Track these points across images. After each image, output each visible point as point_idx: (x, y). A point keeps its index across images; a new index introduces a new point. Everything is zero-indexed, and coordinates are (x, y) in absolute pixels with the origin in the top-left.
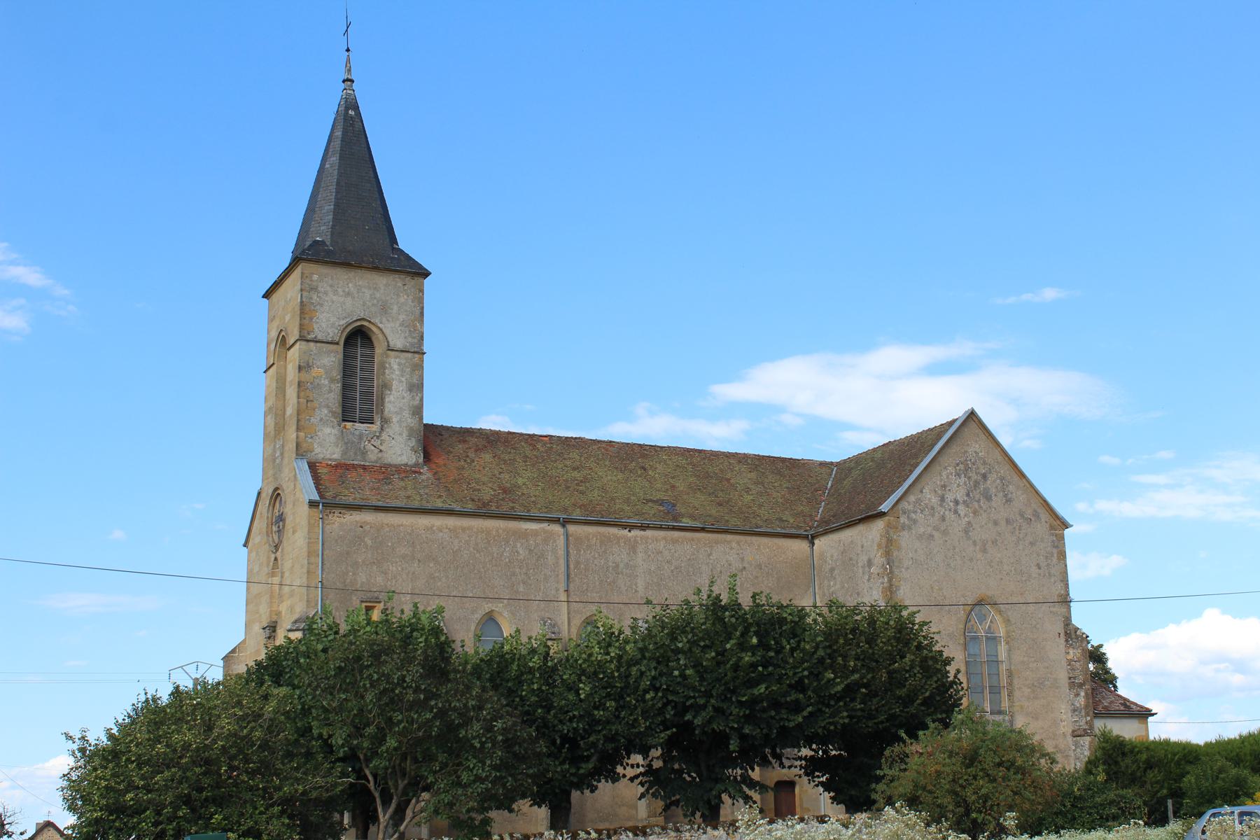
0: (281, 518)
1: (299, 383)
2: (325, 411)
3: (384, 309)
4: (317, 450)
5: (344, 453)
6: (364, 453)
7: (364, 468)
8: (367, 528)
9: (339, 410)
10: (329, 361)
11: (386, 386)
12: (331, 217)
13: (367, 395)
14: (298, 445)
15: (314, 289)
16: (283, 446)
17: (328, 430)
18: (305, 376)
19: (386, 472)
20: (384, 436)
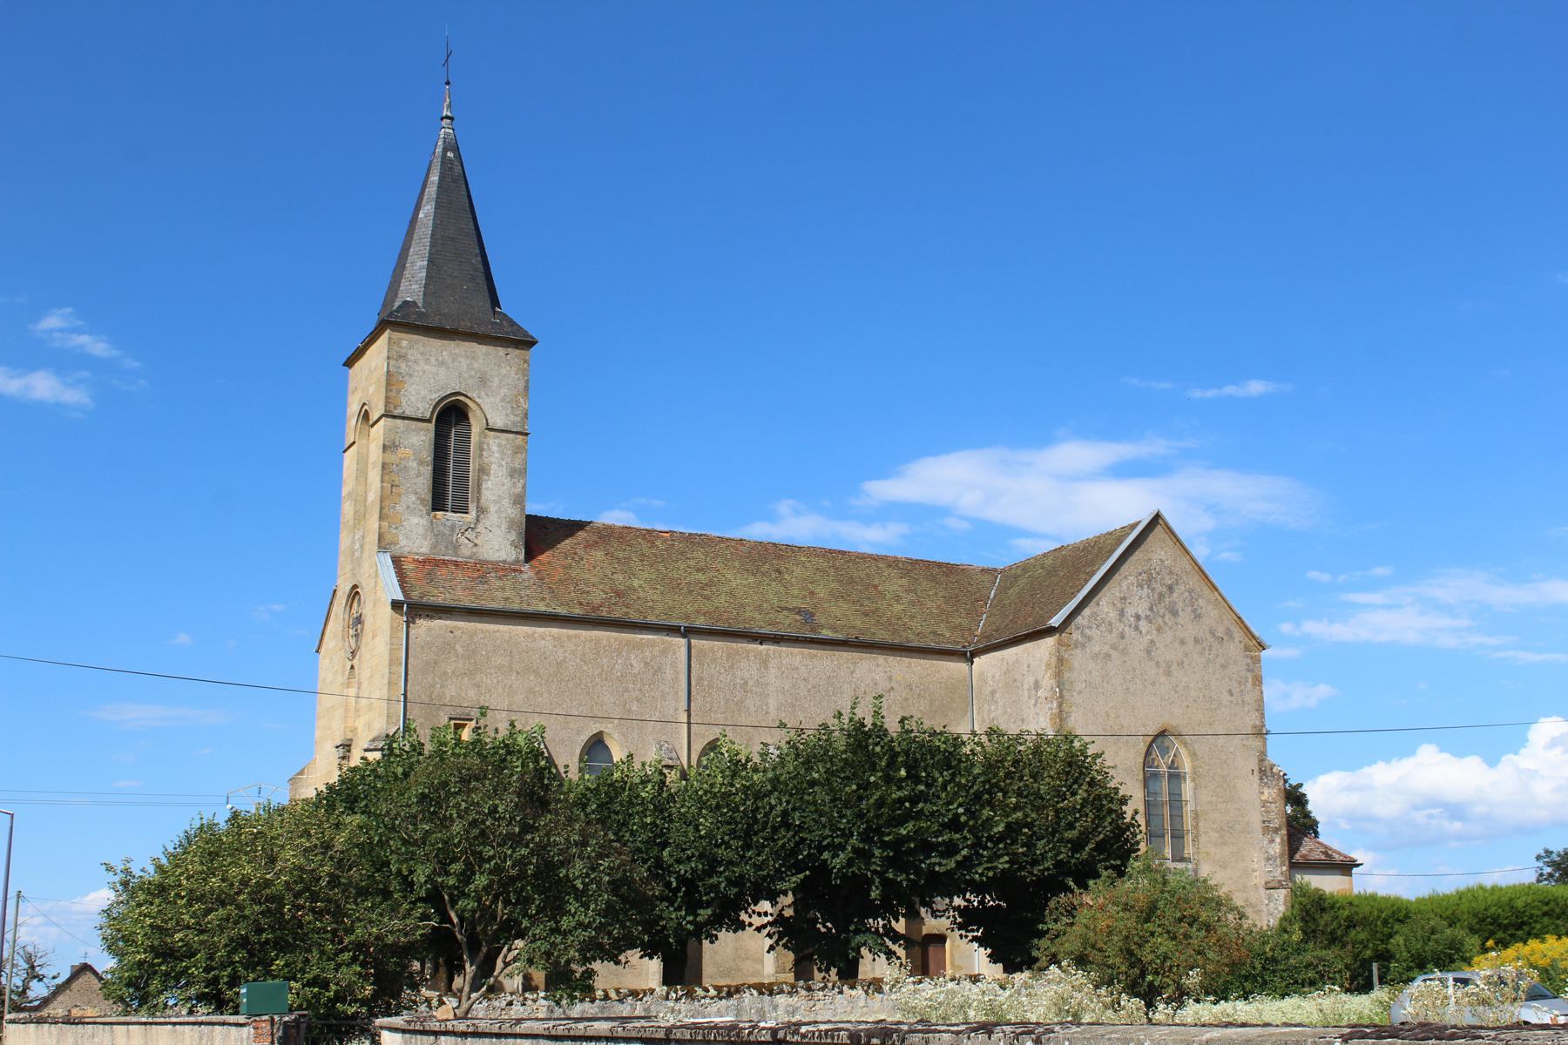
0: (359, 620)
1: (384, 466)
3: (483, 381)
4: (403, 543)
5: (434, 546)
7: (456, 564)
8: (458, 633)
9: (429, 497)
10: (421, 440)
11: (483, 471)
12: (424, 274)
13: (462, 480)
15: (402, 357)
17: (415, 520)
18: (390, 457)
19: (481, 570)
20: (480, 528)
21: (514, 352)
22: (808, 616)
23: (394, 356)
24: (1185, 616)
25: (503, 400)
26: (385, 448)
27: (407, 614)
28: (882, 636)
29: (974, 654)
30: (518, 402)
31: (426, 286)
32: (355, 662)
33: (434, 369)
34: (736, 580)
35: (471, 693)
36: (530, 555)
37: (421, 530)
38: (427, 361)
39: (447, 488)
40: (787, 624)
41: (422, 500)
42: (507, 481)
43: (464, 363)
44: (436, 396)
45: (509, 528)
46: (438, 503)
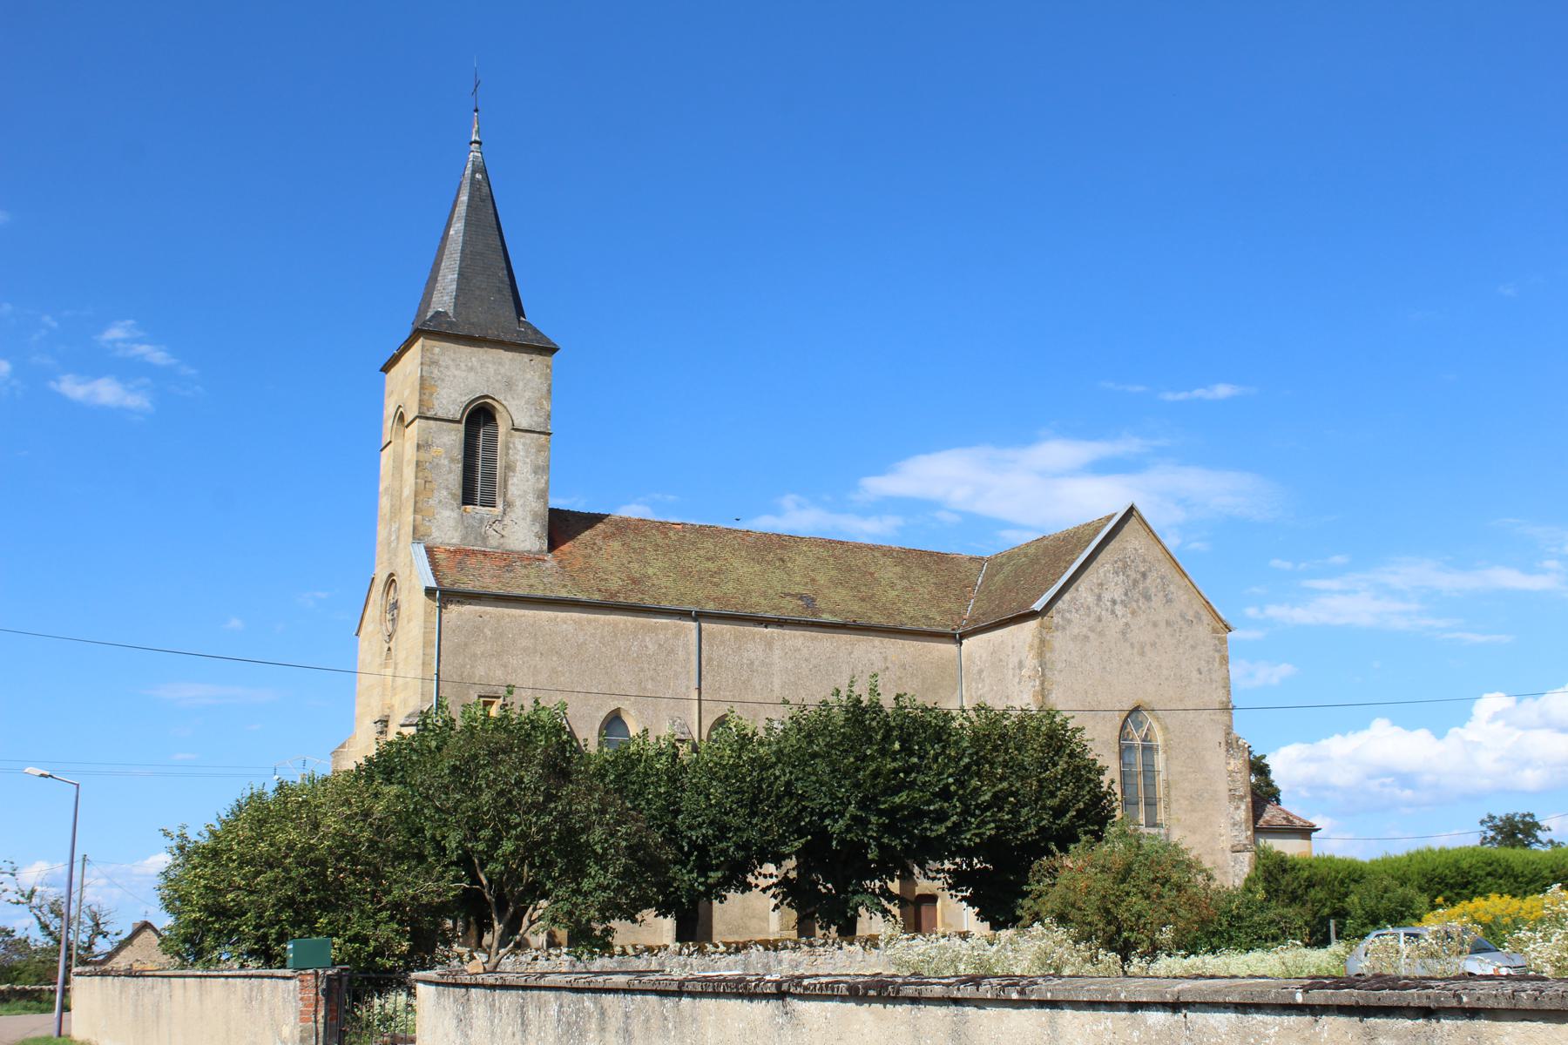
0: (395, 606)
1: (418, 464)
2: (445, 493)
3: (509, 385)
4: (435, 533)
5: (464, 538)
6: (485, 538)
7: (485, 554)
8: (486, 618)
10: (453, 438)
11: (509, 467)
13: (490, 477)
14: (415, 529)
15: (434, 363)
17: (447, 513)
18: (424, 456)
19: (508, 559)
20: (507, 520)
22: (809, 602)
23: (427, 362)
24: (1157, 601)
26: (419, 447)
28: (878, 619)
29: (963, 636)
31: (457, 297)
32: (392, 644)
34: (743, 568)
35: (499, 673)
37: (452, 523)
38: (458, 366)
39: (476, 485)
40: (790, 609)
41: (453, 495)
42: (531, 477)
44: (466, 399)
45: (534, 521)
46: (468, 498)
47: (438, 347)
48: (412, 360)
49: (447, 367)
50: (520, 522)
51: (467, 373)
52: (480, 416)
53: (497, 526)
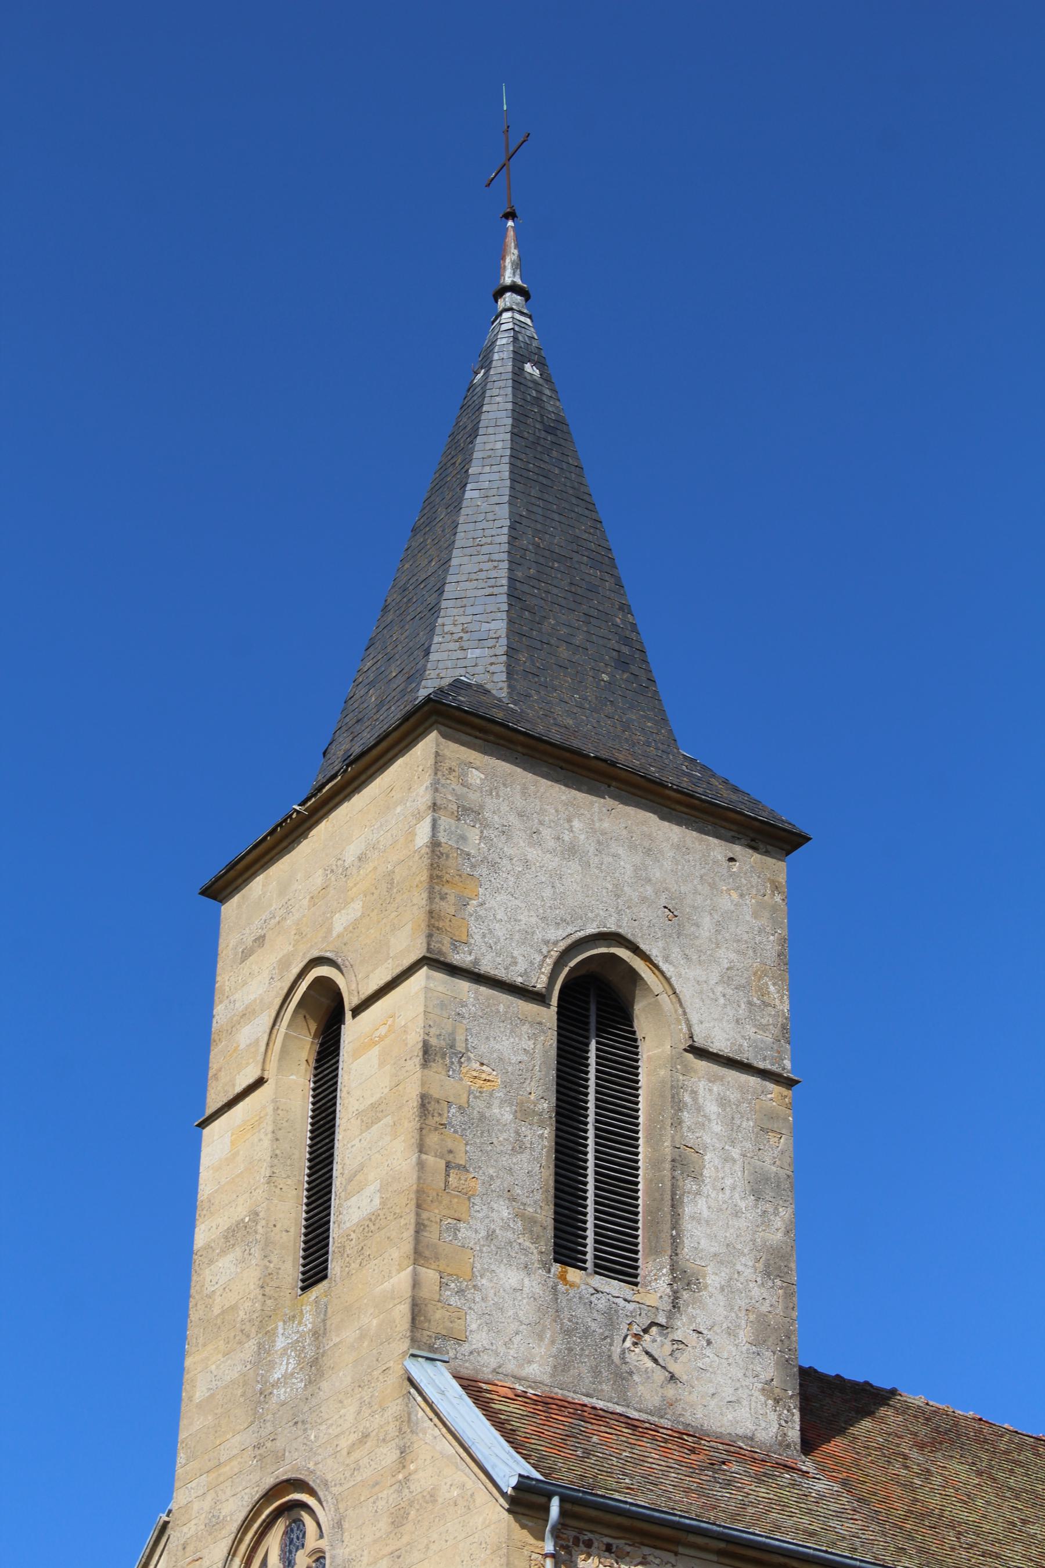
1: (425, 1104)
2: (503, 1211)
4: (479, 1339)
5: (562, 1365)
6: (622, 1376)
7: (632, 1425)
10: (522, 1045)
11: (683, 1164)
13: (620, 1184)
14: (417, 1312)
15: (466, 811)
16: (318, 1334)
17: (511, 1277)
18: (443, 1084)
20: (682, 1330)
21: (749, 859)
25: (726, 979)
26: (428, 1053)
27: (557, 1534)
30: (763, 992)
31: (511, 652)
33: (553, 862)
36: (808, 1446)
37: (526, 1310)
39: (595, 1208)
41: (530, 1222)
43: (627, 863)
44: (560, 936)
45: (758, 1342)
47: (480, 770)
48: (408, 781)
49: (505, 831)
50: (720, 1339)
51: (566, 867)
52: (595, 999)
53: (653, 1341)
